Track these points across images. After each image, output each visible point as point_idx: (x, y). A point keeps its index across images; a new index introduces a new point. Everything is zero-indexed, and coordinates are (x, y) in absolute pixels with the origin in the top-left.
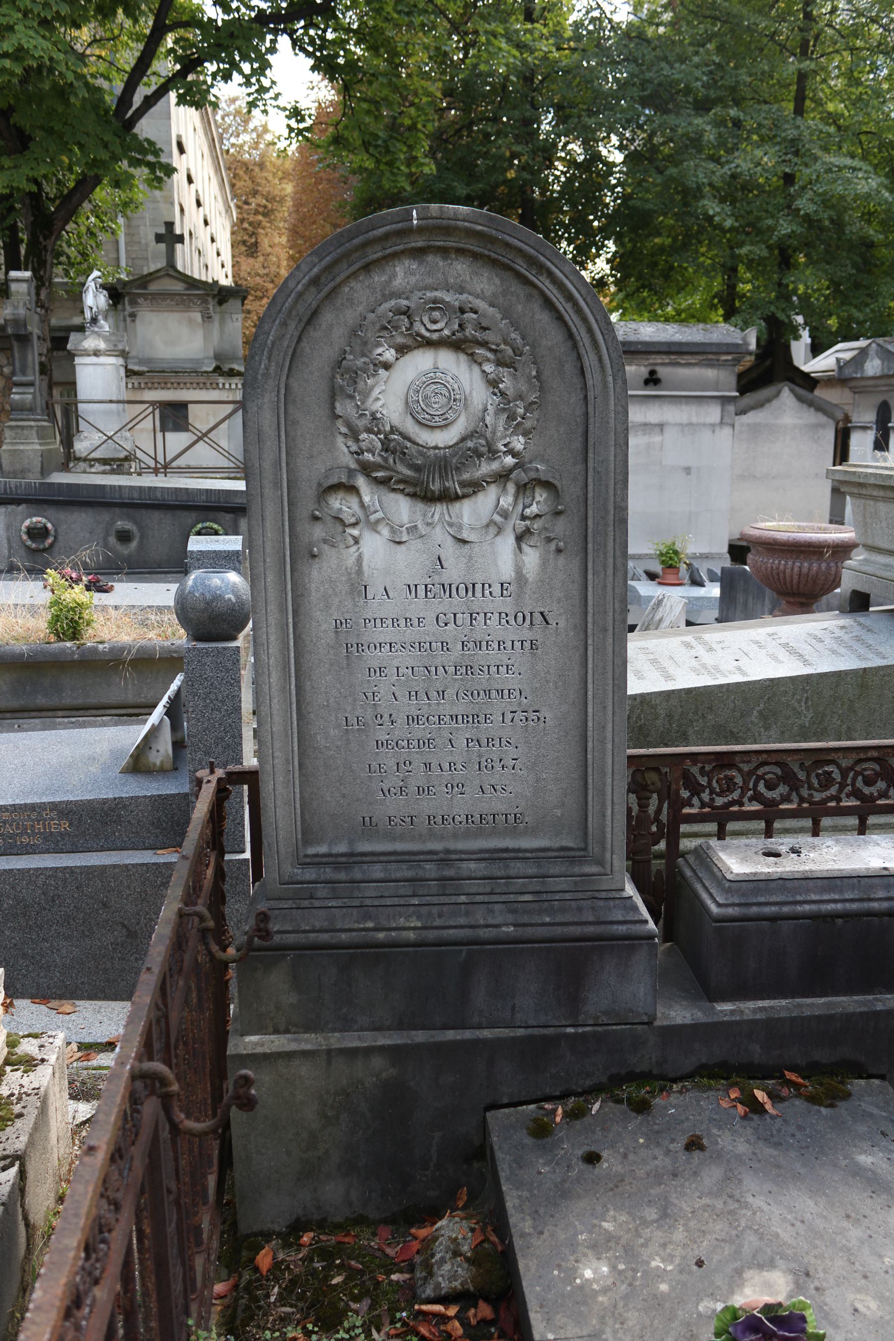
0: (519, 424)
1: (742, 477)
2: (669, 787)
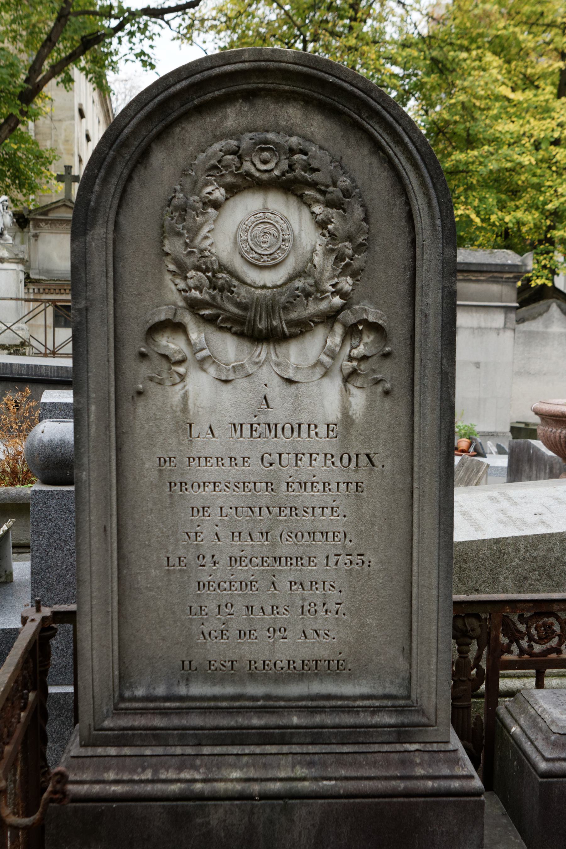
0: (348, 265)
1: (519, 374)
2: (489, 634)
